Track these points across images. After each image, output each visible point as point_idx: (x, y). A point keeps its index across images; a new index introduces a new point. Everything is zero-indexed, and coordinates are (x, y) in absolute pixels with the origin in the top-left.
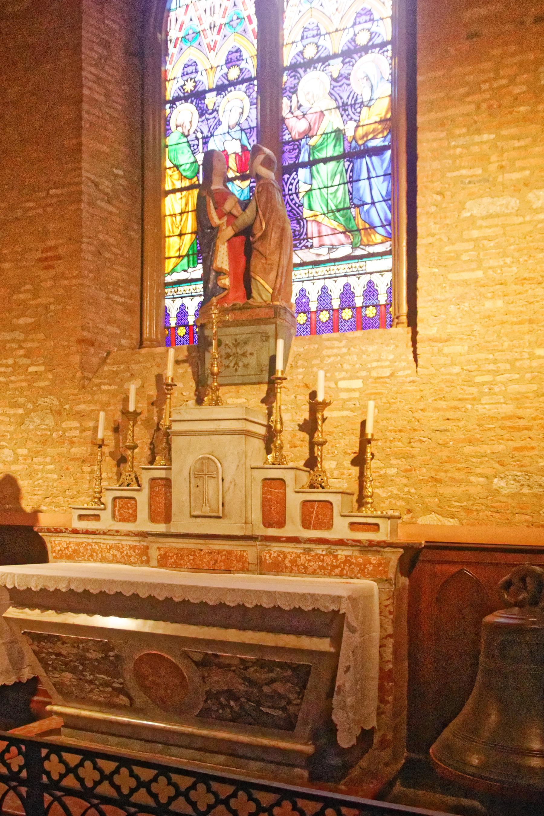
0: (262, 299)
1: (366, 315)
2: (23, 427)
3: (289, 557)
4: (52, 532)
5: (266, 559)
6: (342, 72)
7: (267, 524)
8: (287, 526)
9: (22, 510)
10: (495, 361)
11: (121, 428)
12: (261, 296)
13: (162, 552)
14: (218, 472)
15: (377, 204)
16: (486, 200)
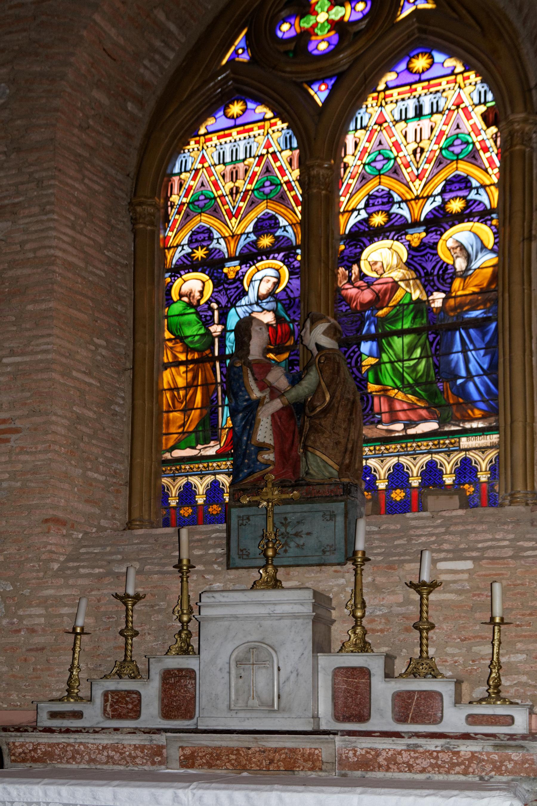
3: (384, 754)
5: (347, 757)
8: (371, 721)
13: (188, 752)
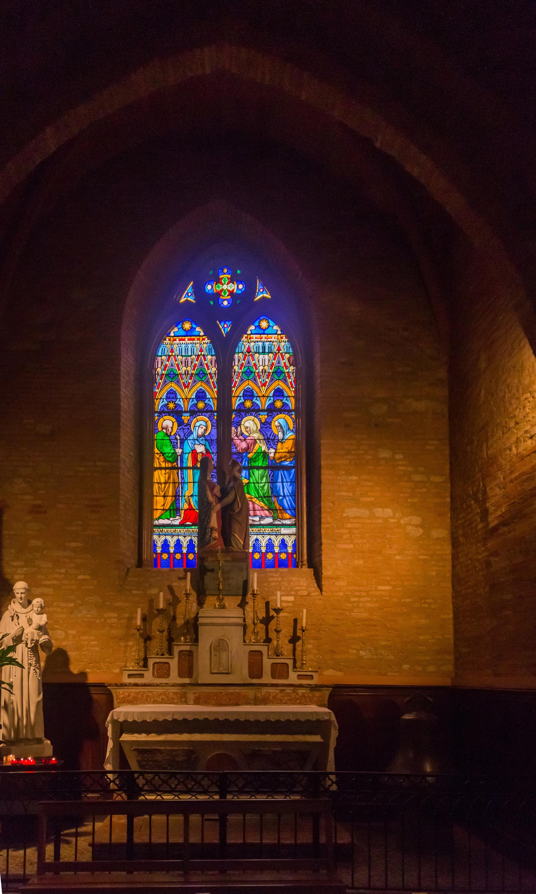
0: (238, 547)
1: (281, 558)
2: (72, 616)
3: (272, 694)
4: (119, 686)
5: (259, 697)
6: (267, 420)
7: (252, 676)
9: (71, 673)
10: (360, 591)
11: (147, 618)
12: (237, 545)
13: (197, 695)
14: (228, 648)
15: (287, 497)
16: (355, 509)
